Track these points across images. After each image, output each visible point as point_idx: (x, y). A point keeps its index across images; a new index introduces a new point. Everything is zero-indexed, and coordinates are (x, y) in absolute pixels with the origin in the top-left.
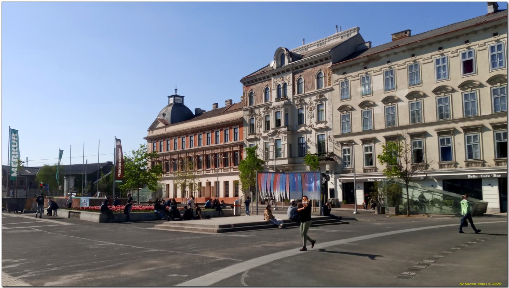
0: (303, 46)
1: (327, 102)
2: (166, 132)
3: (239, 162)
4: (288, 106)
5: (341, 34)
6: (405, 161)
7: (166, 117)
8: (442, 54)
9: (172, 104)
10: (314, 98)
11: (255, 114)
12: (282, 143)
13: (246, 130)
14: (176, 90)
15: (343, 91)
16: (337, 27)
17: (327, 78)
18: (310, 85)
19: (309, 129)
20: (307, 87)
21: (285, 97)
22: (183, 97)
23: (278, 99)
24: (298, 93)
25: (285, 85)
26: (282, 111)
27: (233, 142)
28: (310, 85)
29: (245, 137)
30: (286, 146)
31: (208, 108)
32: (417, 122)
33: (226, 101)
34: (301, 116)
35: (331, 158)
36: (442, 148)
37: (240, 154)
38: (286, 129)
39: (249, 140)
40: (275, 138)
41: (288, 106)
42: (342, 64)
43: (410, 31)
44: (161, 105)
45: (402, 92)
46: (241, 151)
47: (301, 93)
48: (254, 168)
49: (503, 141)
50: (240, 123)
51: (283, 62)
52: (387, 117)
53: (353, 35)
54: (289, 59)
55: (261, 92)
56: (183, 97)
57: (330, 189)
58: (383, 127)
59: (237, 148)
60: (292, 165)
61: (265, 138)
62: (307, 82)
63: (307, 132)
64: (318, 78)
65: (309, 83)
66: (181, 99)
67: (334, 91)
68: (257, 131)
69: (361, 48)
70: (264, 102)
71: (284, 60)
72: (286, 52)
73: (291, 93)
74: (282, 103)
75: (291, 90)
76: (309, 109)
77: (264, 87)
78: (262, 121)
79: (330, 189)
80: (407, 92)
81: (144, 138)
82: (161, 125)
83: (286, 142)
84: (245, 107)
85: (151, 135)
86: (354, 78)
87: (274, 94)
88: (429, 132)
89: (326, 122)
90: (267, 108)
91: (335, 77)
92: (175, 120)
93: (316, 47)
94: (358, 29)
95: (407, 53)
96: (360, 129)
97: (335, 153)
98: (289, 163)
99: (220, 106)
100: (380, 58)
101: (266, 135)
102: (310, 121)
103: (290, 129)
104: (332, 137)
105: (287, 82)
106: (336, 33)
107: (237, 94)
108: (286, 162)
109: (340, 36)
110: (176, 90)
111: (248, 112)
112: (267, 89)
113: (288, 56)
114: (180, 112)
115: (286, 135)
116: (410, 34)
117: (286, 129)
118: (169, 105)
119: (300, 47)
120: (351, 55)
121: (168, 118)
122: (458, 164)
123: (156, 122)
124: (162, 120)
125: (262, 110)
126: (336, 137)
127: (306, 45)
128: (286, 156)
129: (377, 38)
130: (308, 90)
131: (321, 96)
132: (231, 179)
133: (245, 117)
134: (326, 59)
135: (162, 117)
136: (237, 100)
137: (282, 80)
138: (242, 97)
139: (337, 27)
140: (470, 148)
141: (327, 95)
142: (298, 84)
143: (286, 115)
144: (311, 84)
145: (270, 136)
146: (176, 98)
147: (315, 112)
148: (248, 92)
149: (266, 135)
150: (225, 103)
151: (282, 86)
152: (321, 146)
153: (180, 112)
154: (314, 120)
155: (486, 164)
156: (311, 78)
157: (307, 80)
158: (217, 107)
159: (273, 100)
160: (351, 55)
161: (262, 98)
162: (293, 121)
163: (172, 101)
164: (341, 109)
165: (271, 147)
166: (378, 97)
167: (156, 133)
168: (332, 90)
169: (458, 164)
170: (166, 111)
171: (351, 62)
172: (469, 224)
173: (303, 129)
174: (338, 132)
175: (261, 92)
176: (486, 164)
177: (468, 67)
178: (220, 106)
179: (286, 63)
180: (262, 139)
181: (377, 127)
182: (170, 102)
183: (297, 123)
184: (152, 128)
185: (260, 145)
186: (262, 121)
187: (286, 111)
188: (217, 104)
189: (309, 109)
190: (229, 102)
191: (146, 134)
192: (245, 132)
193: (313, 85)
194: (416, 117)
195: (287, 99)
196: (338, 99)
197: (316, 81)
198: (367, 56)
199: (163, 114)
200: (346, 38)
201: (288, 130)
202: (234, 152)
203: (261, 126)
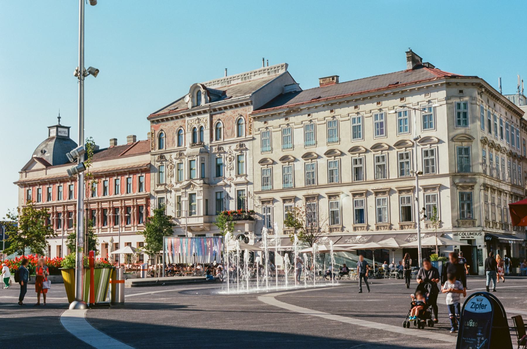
0: (225, 77)
1: (248, 152)
2: (47, 176)
3: (144, 220)
4: (205, 152)
5: (268, 69)
7: (47, 155)
8: (358, 113)
9: (53, 138)
10: (234, 147)
11: (166, 160)
12: (197, 198)
13: (153, 176)
14: (59, 118)
15: (263, 143)
16: (263, 60)
17: (248, 126)
18: (229, 132)
19: (228, 183)
20: (226, 133)
21: (201, 141)
22: (68, 128)
23: (194, 143)
24: (216, 140)
25: (201, 128)
26: (197, 159)
27: (137, 193)
28: (229, 132)
29: (152, 188)
30: (202, 201)
31: (103, 144)
32: (335, 182)
33: (128, 137)
34: (219, 167)
35: (250, 217)
36: (356, 210)
37: (147, 209)
38: (202, 181)
39: (157, 192)
40: (189, 191)
41: (205, 152)
42: (263, 113)
43: (337, 77)
44: (37, 137)
46: (147, 205)
48: (161, 228)
49: (406, 205)
50: (148, 169)
51: (199, 100)
52: (307, 174)
53: (282, 72)
54: (205, 98)
55: (173, 134)
56: (68, 128)
57: (37, 163)
58: (303, 185)
59: (142, 202)
60: (208, 224)
61: (177, 190)
62: (226, 128)
63: (226, 185)
64: (238, 124)
65: (229, 129)
66: (66, 130)
67: (254, 141)
69: (288, 89)
70: (176, 147)
71: (201, 99)
72: (202, 90)
73: (209, 139)
74: (197, 150)
75: (209, 135)
76: (228, 159)
77: (177, 128)
78: (174, 170)
79: (37, 163)
80: (326, 149)
81: (15, 183)
82: (39, 165)
83: (201, 197)
84: (153, 151)
85: (24, 179)
87: (188, 138)
88: (298, 196)
89: (246, 175)
90: (181, 154)
91: (258, 124)
92: (60, 159)
93: (239, 81)
94: (287, 65)
95: (326, 107)
96: (281, 187)
97: (255, 211)
98: (205, 222)
99: (119, 144)
100: (301, 110)
101: (178, 186)
102: (229, 173)
103: (206, 181)
104: (252, 193)
105: (202, 125)
106: (263, 68)
107: (143, 131)
108: (201, 220)
109: (266, 71)
110: (59, 118)
111: (156, 157)
112: (180, 131)
113: (205, 94)
114: (62, 147)
115: (202, 189)
116: (337, 81)
117: (202, 181)
118: (50, 139)
119: (222, 78)
120: (278, 97)
121: (49, 157)
122: (370, 226)
123: (32, 163)
124: (41, 160)
125: (174, 155)
126: (256, 193)
127: (229, 77)
128: (202, 214)
129: (307, 81)
131: (241, 146)
132: (135, 240)
133: (153, 163)
134: (247, 104)
135: (39, 155)
136: (143, 137)
137: (199, 123)
138: (149, 134)
139: (263, 60)
140: (380, 211)
141: (247, 144)
142: (217, 129)
143: (202, 165)
144: (231, 130)
145: (183, 188)
146: (60, 129)
147: (234, 162)
148: (157, 133)
149: (178, 186)
150: (126, 139)
151: (198, 130)
152: (241, 203)
153: (62, 147)
154: (234, 173)
155: (393, 227)
156: (231, 123)
157: (226, 126)
158: (116, 144)
159: (188, 145)
160: (278, 97)
161: (174, 142)
162: (212, 172)
163: (53, 133)
164: (263, 161)
165: (184, 202)
167: (32, 176)
168: (254, 139)
169: (370, 226)
170: (46, 147)
171: (271, 111)
173: (221, 183)
174: (259, 188)
175: (173, 134)
176: (393, 227)
177: (380, 129)
178: (119, 144)
179: (203, 103)
180: (173, 192)
181: (298, 185)
182: (52, 135)
183: (215, 175)
184: (26, 169)
185: (171, 198)
186: (174, 170)
187: (202, 159)
188: (115, 140)
189: (228, 159)
190: (132, 139)
191: (18, 178)
192: (152, 182)
193: (233, 132)
194: (311, 180)
195: (204, 146)
196: (258, 150)
197: (236, 127)
198: (288, 107)
199: (42, 151)
200: (273, 76)
201: (204, 183)
202: (139, 207)
203: (172, 176)
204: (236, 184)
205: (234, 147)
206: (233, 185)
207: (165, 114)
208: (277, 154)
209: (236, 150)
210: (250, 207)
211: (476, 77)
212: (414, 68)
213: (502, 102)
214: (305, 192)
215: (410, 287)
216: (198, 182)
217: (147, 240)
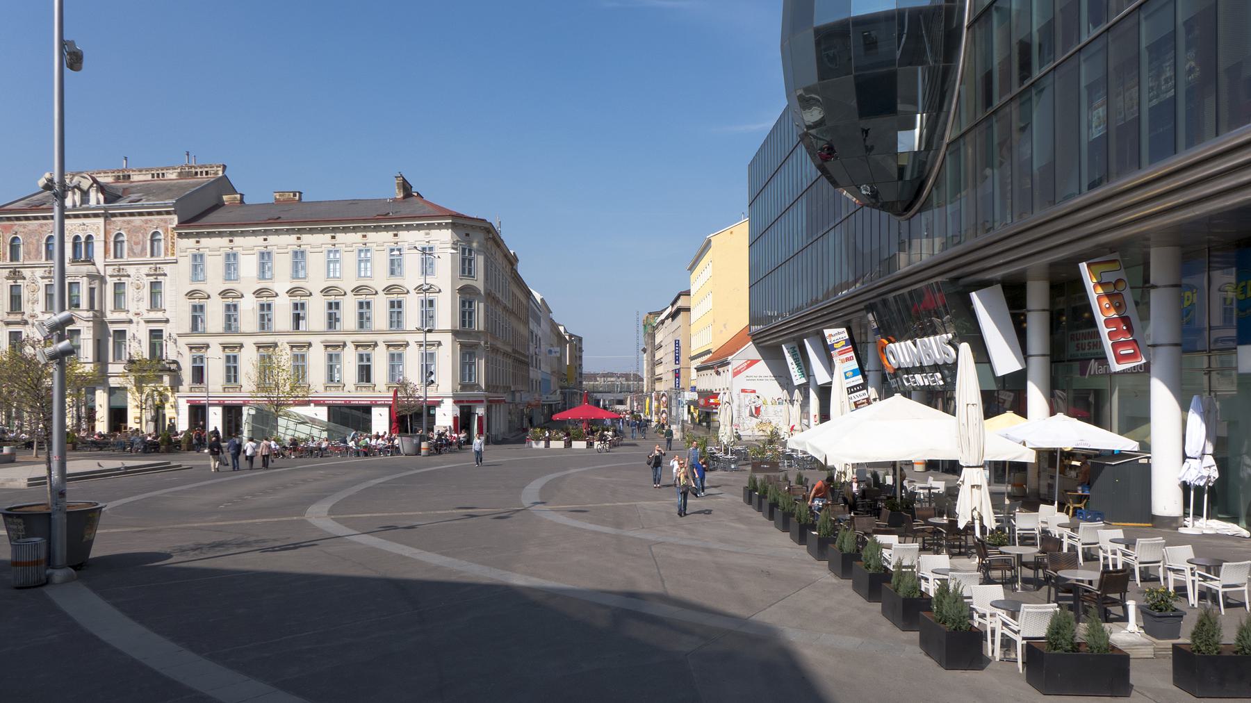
6: (284, 377)
18: (138, 249)
25: (89, 237)
28: (138, 249)
45: (281, 284)
47: (159, 255)
65: (137, 244)
68: (26, 308)
86: (214, 246)
102: (137, 301)
129: (256, 189)
130: (135, 255)
142: (116, 243)
144: (140, 247)
151: (83, 239)
164: (191, 294)
166: (281, 284)
172: (1014, 41)
179: (93, 202)
193: (144, 249)
197: (149, 243)
201: (95, 316)
203: (36, 302)
204: (148, 322)
205: (145, 269)
206: (142, 322)
207: (11, 211)
208: (348, 284)
209: (43, 278)
210: (170, 352)
211: (484, 220)
212: (404, 198)
213: (502, 250)
214: (420, 337)
215: (975, 490)
216: (85, 314)
217: (784, 444)
